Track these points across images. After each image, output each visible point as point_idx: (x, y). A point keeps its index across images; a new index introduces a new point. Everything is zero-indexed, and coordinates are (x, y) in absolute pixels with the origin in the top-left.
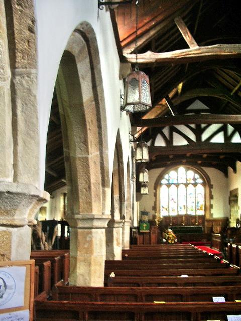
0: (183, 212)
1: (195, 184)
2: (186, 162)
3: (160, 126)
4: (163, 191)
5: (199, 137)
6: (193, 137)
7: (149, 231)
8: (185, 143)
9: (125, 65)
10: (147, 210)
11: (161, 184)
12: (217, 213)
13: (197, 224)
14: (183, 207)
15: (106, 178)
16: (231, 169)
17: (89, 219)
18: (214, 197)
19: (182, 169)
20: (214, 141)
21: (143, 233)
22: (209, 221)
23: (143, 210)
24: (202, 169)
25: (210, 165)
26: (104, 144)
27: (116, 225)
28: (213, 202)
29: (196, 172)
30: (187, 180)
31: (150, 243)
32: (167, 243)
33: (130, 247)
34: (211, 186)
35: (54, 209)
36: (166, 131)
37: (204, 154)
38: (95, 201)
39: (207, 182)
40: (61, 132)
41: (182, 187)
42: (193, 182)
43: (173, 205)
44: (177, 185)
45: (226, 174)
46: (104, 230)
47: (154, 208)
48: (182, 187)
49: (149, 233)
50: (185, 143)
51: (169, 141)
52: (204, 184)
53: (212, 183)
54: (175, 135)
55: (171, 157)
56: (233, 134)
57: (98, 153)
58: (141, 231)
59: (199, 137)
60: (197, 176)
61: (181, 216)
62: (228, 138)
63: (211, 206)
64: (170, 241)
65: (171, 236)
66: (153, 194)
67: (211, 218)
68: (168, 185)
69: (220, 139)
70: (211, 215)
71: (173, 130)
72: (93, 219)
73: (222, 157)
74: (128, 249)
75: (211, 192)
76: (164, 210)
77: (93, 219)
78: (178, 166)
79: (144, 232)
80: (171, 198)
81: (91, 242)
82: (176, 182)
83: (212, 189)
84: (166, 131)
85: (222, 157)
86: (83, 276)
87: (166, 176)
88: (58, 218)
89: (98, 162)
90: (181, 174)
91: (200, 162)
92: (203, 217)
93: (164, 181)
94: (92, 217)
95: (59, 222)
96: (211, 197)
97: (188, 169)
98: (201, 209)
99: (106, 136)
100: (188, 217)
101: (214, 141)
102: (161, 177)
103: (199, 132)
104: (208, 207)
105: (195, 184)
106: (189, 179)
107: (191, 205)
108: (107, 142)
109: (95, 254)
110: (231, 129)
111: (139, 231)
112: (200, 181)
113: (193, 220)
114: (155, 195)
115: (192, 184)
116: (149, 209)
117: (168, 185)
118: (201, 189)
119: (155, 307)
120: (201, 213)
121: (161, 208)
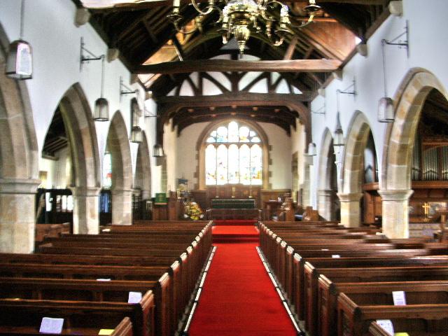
0: (234, 181)
1: (250, 145)
2: (237, 115)
3: (188, 72)
4: (209, 151)
5: (235, 85)
6: (227, 84)
7: (165, 204)
8: (218, 92)
9: (81, 10)
10: (186, 178)
11: (206, 145)
12: (278, 184)
13: (250, 197)
14: (234, 174)
15: (33, 141)
16: (292, 127)
17: (10, 183)
18: (274, 161)
19: (233, 124)
20: (253, 90)
21: (159, 206)
22: (266, 193)
23: (181, 178)
24: (258, 125)
25: (267, 120)
26: (26, 105)
27: (90, 194)
28: (273, 168)
29: (251, 129)
30: (240, 139)
31: (168, 219)
32: (189, 219)
33: (133, 223)
34: (269, 148)
35: (57, 174)
36: (194, 77)
37: (190, 108)
38: (20, 165)
39: (265, 143)
40: (374, 7)
41: (233, 147)
42: (248, 141)
43: (222, 171)
44: (227, 145)
45: (289, 133)
46: (34, 195)
47: (197, 175)
48: (233, 147)
49: (166, 207)
50: (218, 92)
51: (198, 90)
52: (261, 145)
53: (271, 143)
54: (206, 81)
55: (213, 108)
56: (279, 81)
57: (20, 115)
58: (156, 204)
59: (235, 85)
60: (253, 134)
61: (230, 186)
62: (272, 87)
63: (270, 174)
64: (192, 217)
65: (194, 211)
66: (194, 157)
67: (270, 191)
68: (216, 145)
69: (261, 88)
70: (270, 185)
71: (203, 75)
72: (14, 184)
73: (277, 110)
74: (130, 224)
75: (269, 155)
76: (211, 177)
77: (14, 184)
78: (227, 121)
79: (159, 205)
80: (218, 163)
81: (14, 208)
82: (225, 140)
83: (271, 152)
84: (194, 77)
85: (277, 110)
86: (6, 243)
87: (213, 134)
88: (63, 185)
89: (21, 122)
90: (233, 130)
91: (253, 116)
92: (258, 188)
93: (210, 140)
94: (13, 182)
95: (48, 191)
96: (270, 162)
97: (240, 125)
98: (258, 178)
99: (28, 97)
100: (240, 188)
101: (253, 90)
102: (205, 134)
103: (235, 78)
104: (267, 175)
105: (250, 145)
106: (241, 138)
107: (245, 173)
108: (29, 102)
109: (19, 221)
110: (275, 76)
111: (153, 203)
112: (257, 140)
113: (246, 193)
114: (198, 157)
115: (247, 144)
116: (189, 176)
117: (216, 145)
118: (258, 151)
119: (97, 285)
120: (258, 182)
121: (207, 175)
